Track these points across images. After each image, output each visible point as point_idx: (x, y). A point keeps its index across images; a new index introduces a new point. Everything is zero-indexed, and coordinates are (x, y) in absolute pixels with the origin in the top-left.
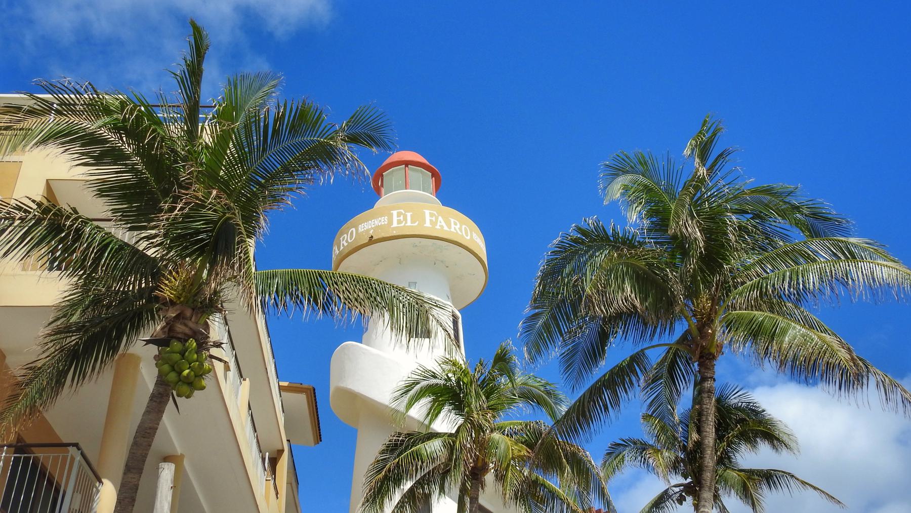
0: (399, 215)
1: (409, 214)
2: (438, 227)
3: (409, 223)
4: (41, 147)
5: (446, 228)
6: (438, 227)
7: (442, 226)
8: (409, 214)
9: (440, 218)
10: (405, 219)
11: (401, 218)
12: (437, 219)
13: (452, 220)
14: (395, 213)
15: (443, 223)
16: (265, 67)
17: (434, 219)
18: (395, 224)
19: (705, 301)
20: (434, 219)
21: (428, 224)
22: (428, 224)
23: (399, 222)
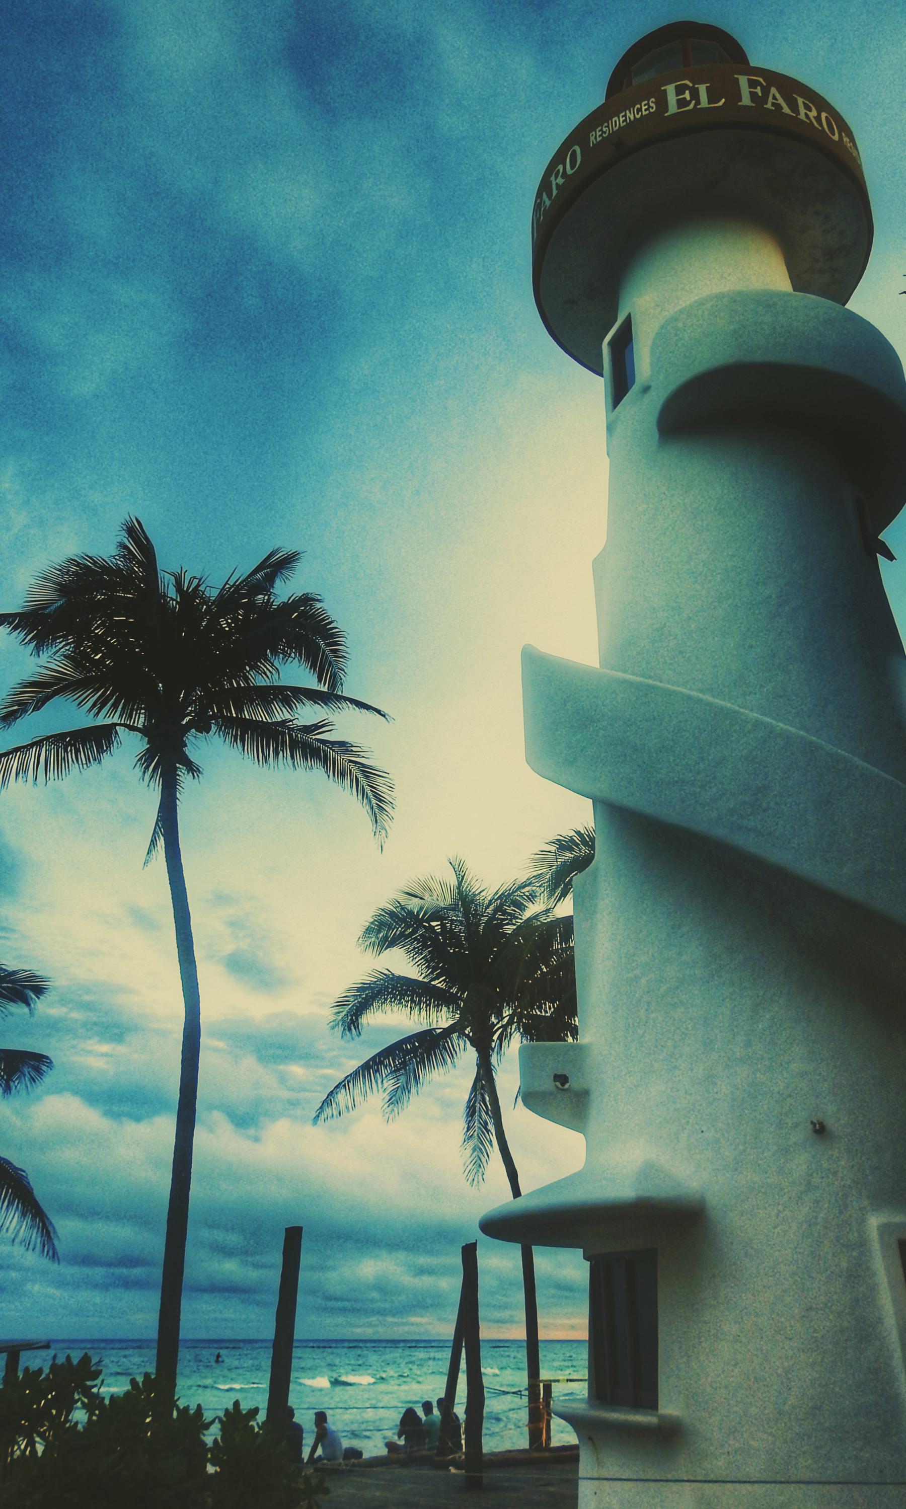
0: (680, 90)
1: (702, 89)
2: (769, 106)
3: (704, 102)
4: (38, 973)
5: (786, 110)
6: (769, 106)
7: (778, 107)
8: (702, 89)
9: (773, 90)
10: (695, 95)
11: (687, 95)
12: (766, 91)
13: (800, 101)
14: (670, 89)
15: (781, 101)
16: (557, 1423)
17: (758, 90)
18: (673, 108)
19: (38, 477)
20: (758, 90)
21: (746, 100)
22: (746, 100)
23: (682, 103)
